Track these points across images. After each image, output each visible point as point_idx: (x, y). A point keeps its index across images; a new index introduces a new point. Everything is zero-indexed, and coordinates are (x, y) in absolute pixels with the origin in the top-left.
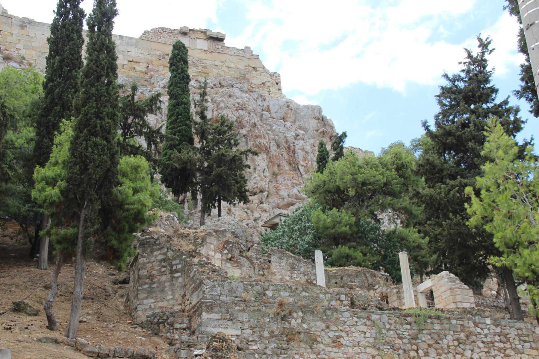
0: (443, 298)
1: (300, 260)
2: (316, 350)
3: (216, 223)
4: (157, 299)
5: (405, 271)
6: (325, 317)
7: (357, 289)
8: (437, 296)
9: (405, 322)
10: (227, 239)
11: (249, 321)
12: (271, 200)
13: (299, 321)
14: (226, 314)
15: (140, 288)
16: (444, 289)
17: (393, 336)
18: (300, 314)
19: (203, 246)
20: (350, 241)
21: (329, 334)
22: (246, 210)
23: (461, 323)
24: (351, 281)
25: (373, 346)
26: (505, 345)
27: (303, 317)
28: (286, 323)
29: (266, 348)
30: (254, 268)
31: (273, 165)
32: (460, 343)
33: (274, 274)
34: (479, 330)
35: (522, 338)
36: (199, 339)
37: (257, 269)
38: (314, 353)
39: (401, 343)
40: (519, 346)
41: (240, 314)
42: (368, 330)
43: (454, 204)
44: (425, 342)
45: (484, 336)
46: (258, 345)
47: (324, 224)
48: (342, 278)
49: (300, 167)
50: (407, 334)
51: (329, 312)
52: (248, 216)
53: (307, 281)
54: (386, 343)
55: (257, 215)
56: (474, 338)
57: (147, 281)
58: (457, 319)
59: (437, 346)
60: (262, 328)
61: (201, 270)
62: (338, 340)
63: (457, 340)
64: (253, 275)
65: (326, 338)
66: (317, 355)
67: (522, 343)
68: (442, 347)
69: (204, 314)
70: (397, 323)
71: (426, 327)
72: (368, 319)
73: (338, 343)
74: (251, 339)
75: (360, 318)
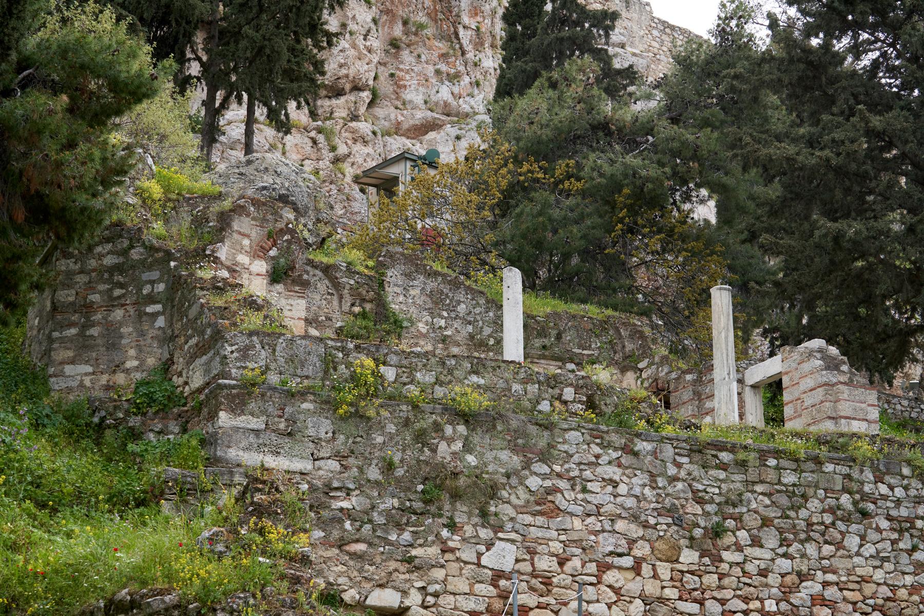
0: (806, 404)
4: (98, 365)
5: (723, 334)
12: (379, 112)
13: (458, 446)
15: (56, 334)
16: (809, 383)
17: (682, 495)
19: (222, 241)
22: (313, 134)
23: (846, 470)
25: (633, 516)
30: (341, 297)
31: (392, 22)
37: (348, 300)
39: (700, 512)
42: (625, 479)
49: (461, 32)
53: (471, 337)
57: (75, 318)
62: (550, 498)
66: (496, 533)
68: (794, 526)
69: (224, 419)
72: (628, 450)
74: (336, 484)
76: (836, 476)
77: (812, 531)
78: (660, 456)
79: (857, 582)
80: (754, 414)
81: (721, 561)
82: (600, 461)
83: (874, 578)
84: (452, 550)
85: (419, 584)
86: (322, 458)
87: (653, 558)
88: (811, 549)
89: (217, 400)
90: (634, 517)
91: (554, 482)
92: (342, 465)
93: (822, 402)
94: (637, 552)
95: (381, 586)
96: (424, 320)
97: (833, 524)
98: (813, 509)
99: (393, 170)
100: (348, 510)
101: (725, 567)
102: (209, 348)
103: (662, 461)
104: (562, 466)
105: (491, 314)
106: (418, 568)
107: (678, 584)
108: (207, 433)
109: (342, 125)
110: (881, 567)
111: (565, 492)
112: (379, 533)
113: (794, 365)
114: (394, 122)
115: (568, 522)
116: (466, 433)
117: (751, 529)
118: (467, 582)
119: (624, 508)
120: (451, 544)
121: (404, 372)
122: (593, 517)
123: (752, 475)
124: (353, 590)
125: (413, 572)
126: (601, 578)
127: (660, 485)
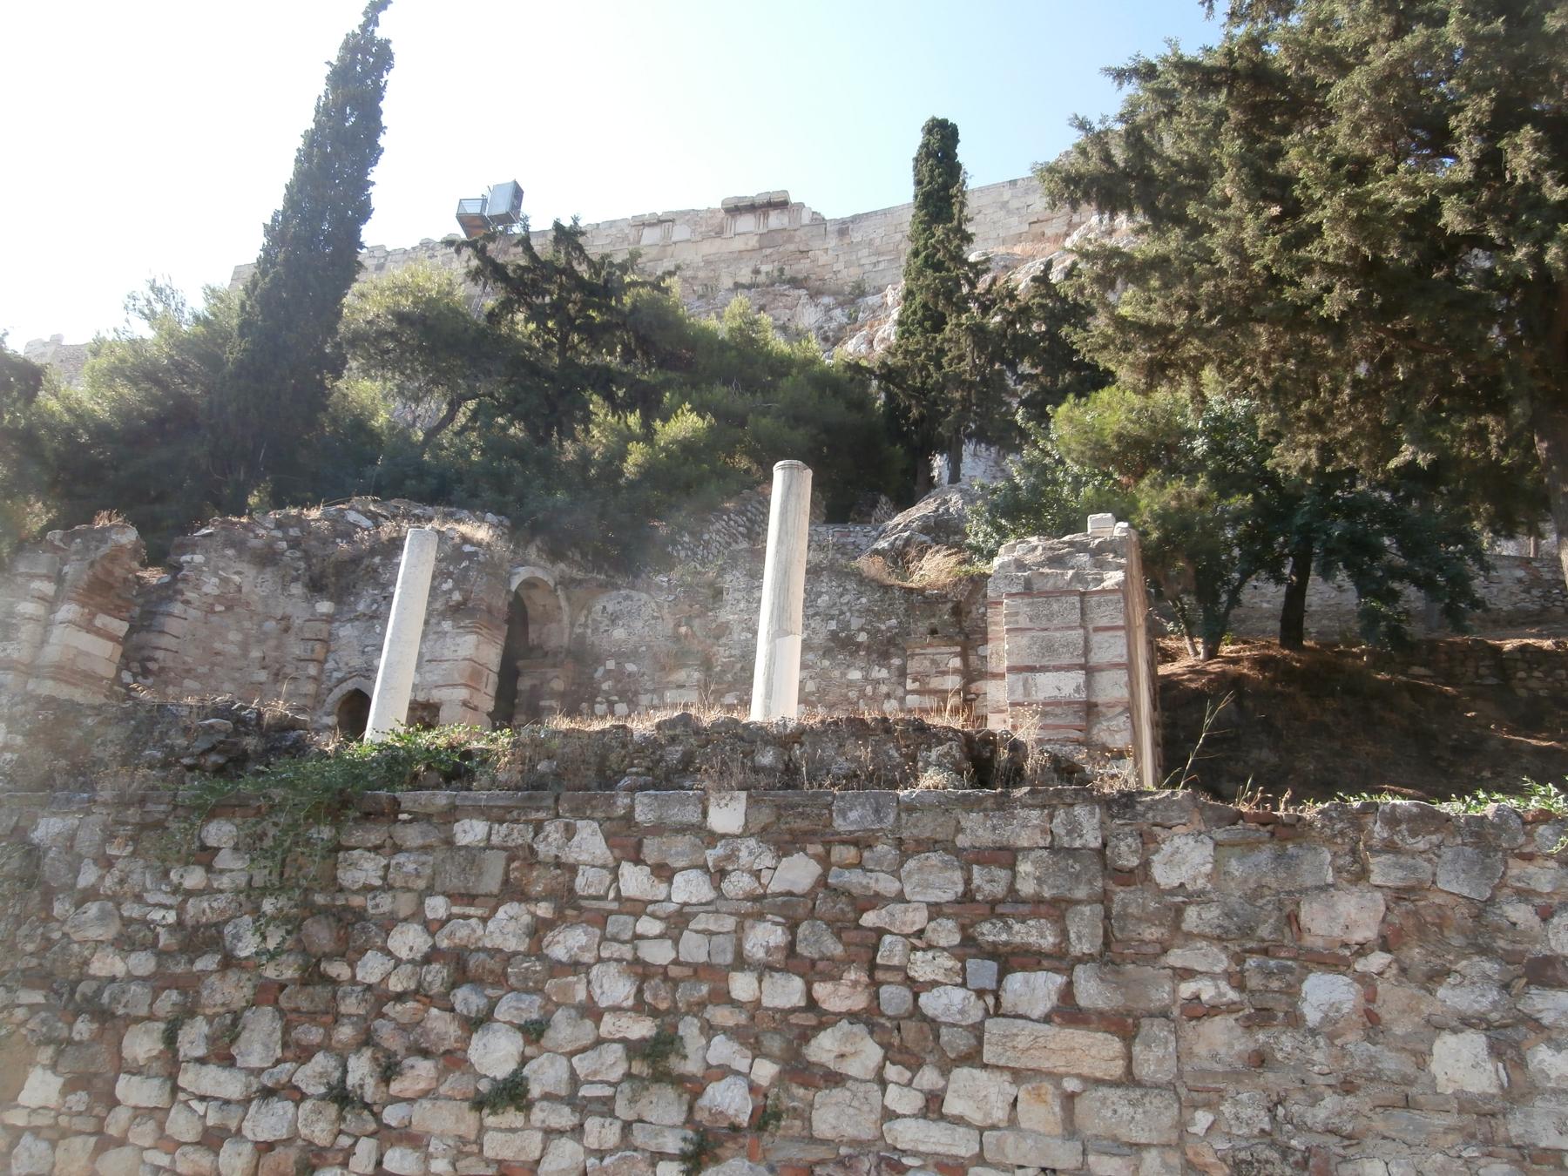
23: (520, 835)
35: (989, 932)
40: (949, 1003)
58: (494, 815)
67: (983, 971)
105: (864, 600)
110: (578, 1131)
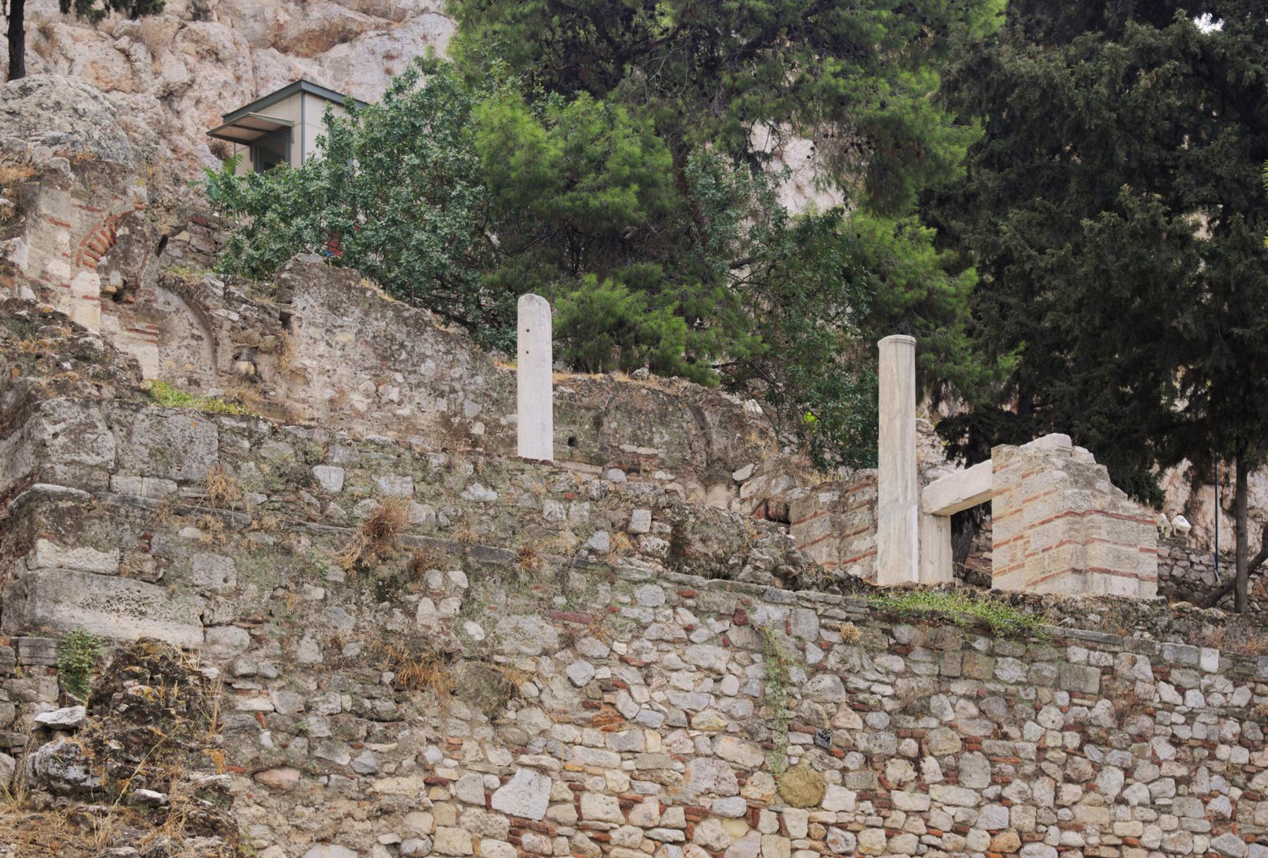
1: (419, 326)
2: (512, 733)
3: (14, 105)
5: (898, 422)
6: (560, 601)
7: (660, 474)
8: (1008, 536)
9: (885, 642)
10: (130, 207)
11: (238, 592)
13: (452, 606)
14: (139, 555)
16: (1043, 509)
17: (830, 697)
18: (459, 577)
19: (20, 232)
20: (640, 257)
21: (571, 671)
22: (124, 42)
23: (1108, 660)
24: (635, 439)
25: (746, 730)
26: (1256, 755)
27: (467, 593)
28: (397, 611)
29: (308, 708)
30: (216, 343)
32: (1087, 740)
33: (300, 375)
34: (1168, 693)
36: (24, 651)
38: (507, 743)
41: (198, 560)
42: (734, 667)
43: (1140, 139)
44: (952, 727)
45: (1182, 719)
46: (275, 694)
47: (528, 163)
48: (598, 423)
50: (889, 690)
51: (577, 580)
52: (135, 73)
53: (445, 420)
54: (798, 724)
55: (175, 72)
56: (1146, 721)
58: (1091, 644)
59: (997, 747)
60: (293, 625)
61: (21, 346)
62: (608, 698)
63: (1080, 727)
64: (207, 375)
65: (558, 686)
66: (516, 754)
69: (45, 550)
70: (855, 644)
71: (967, 669)
72: (739, 618)
73: (605, 709)
74: (243, 668)
75: (708, 613)
76: (1089, 669)
77: (1045, 759)
78: (796, 631)
79: (1116, 846)
80: (936, 564)
81: (891, 807)
82: (692, 637)
83: (1144, 840)
84: (443, 783)
85: (389, 839)
86: (220, 624)
87: (780, 801)
88: (1042, 791)
89: (31, 522)
90: (749, 732)
91: (615, 670)
92: (254, 636)
93: (1062, 544)
94: (752, 791)
95: (324, 841)
96: (362, 387)
97: (1080, 749)
98: (1049, 725)
99: (280, 114)
100: (265, 713)
101: (897, 818)
102: (12, 426)
103: (799, 638)
104: (628, 643)
106: (385, 812)
107: (819, 845)
108: (16, 577)
109: (176, 26)
111: (633, 689)
112: (319, 752)
113: (1015, 479)
114: (271, 23)
115: (637, 739)
116: (465, 585)
117: (944, 756)
118: (469, 836)
119: (732, 718)
120: (441, 773)
121: (356, 476)
122: (680, 732)
123: (951, 667)
124: (276, 847)
125: (377, 818)
126: (691, 833)
127: (794, 679)
